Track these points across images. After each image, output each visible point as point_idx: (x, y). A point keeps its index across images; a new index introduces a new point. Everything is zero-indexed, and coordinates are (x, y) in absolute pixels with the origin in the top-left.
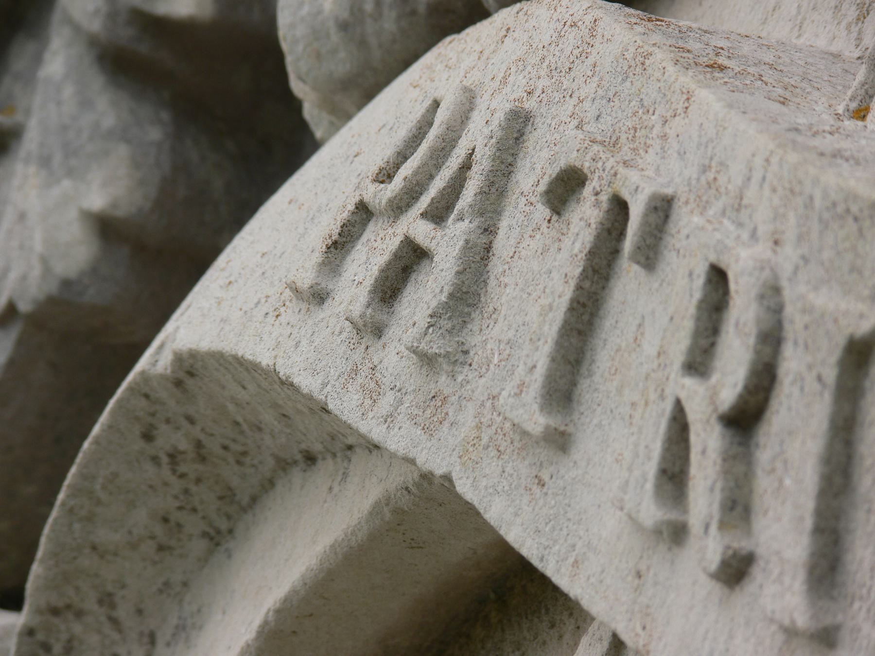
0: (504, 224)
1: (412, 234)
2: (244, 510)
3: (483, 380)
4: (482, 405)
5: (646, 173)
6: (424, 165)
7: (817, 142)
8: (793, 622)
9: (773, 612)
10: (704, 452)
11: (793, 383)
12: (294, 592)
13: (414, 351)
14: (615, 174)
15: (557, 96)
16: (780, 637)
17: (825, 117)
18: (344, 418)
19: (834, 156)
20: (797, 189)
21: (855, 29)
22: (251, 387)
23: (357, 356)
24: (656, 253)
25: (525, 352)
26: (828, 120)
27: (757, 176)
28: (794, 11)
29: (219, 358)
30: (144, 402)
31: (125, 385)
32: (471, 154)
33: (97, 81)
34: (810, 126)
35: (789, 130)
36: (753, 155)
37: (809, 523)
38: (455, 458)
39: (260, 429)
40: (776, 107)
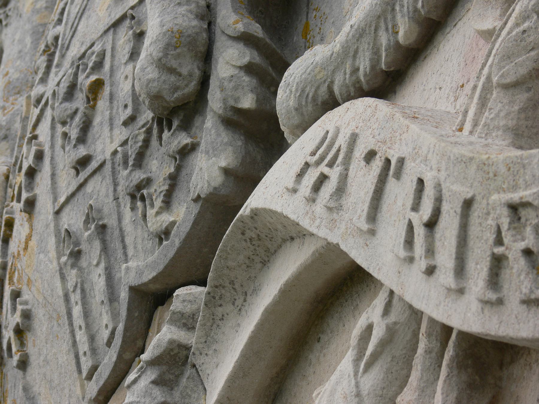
0: (351, 167)
1: (323, 171)
2: (273, 255)
3: (347, 214)
4: (347, 222)
5: (395, 151)
6: (325, 150)
7: (449, 139)
8: (450, 286)
9: (444, 283)
10: (419, 235)
11: (446, 213)
12: (289, 279)
13: (326, 206)
14: (386, 151)
15: (366, 128)
16: (446, 291)
17: (450, 131)
18: (305, 227)
19: (455, 143)
20: (445, 154)
21: (454, 104)
22: (274, 218)
23: (308, 208)
24: (400, 175)
25: (360, 206)
26: (451, 133)
27: (432, 150)
28: (434, 99)
29: (265, 210)
30: (242, 224)
31: (236, 218)
32: (340, 147)
33: (222, 128)
34: (446, 134)
35: (440, 136)
36: (430, 144)
37: (454, 256)
38: (340, 238)
39: (277, 230)
40: (435, 129)
